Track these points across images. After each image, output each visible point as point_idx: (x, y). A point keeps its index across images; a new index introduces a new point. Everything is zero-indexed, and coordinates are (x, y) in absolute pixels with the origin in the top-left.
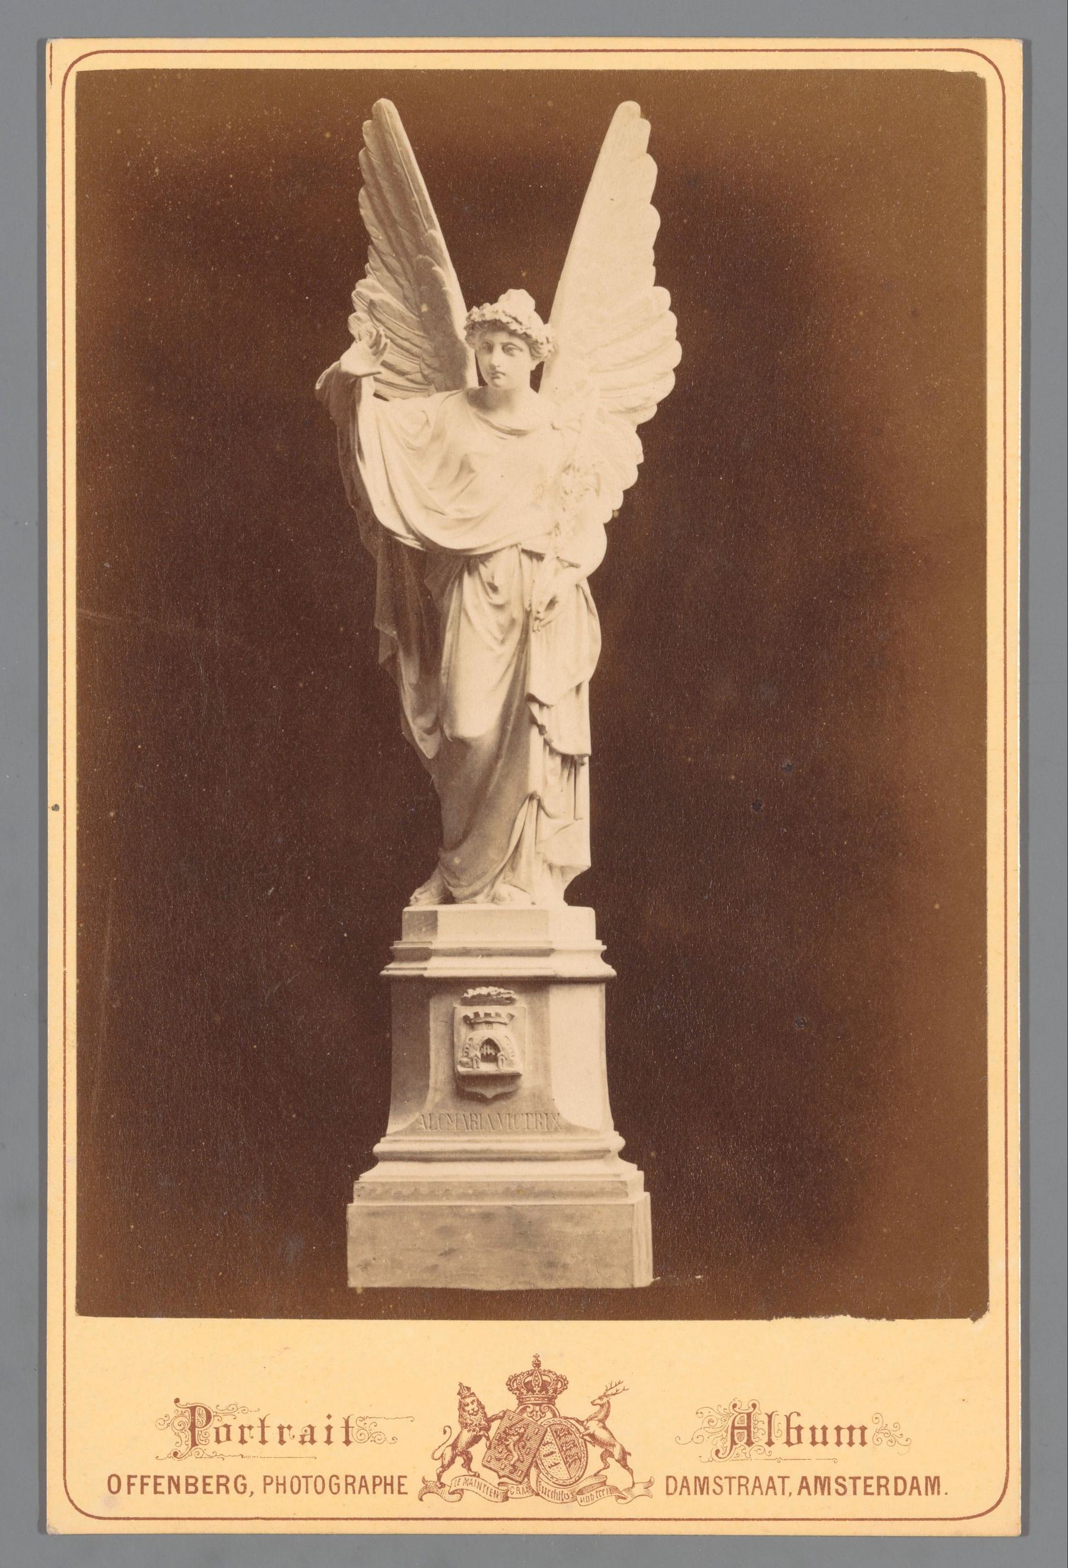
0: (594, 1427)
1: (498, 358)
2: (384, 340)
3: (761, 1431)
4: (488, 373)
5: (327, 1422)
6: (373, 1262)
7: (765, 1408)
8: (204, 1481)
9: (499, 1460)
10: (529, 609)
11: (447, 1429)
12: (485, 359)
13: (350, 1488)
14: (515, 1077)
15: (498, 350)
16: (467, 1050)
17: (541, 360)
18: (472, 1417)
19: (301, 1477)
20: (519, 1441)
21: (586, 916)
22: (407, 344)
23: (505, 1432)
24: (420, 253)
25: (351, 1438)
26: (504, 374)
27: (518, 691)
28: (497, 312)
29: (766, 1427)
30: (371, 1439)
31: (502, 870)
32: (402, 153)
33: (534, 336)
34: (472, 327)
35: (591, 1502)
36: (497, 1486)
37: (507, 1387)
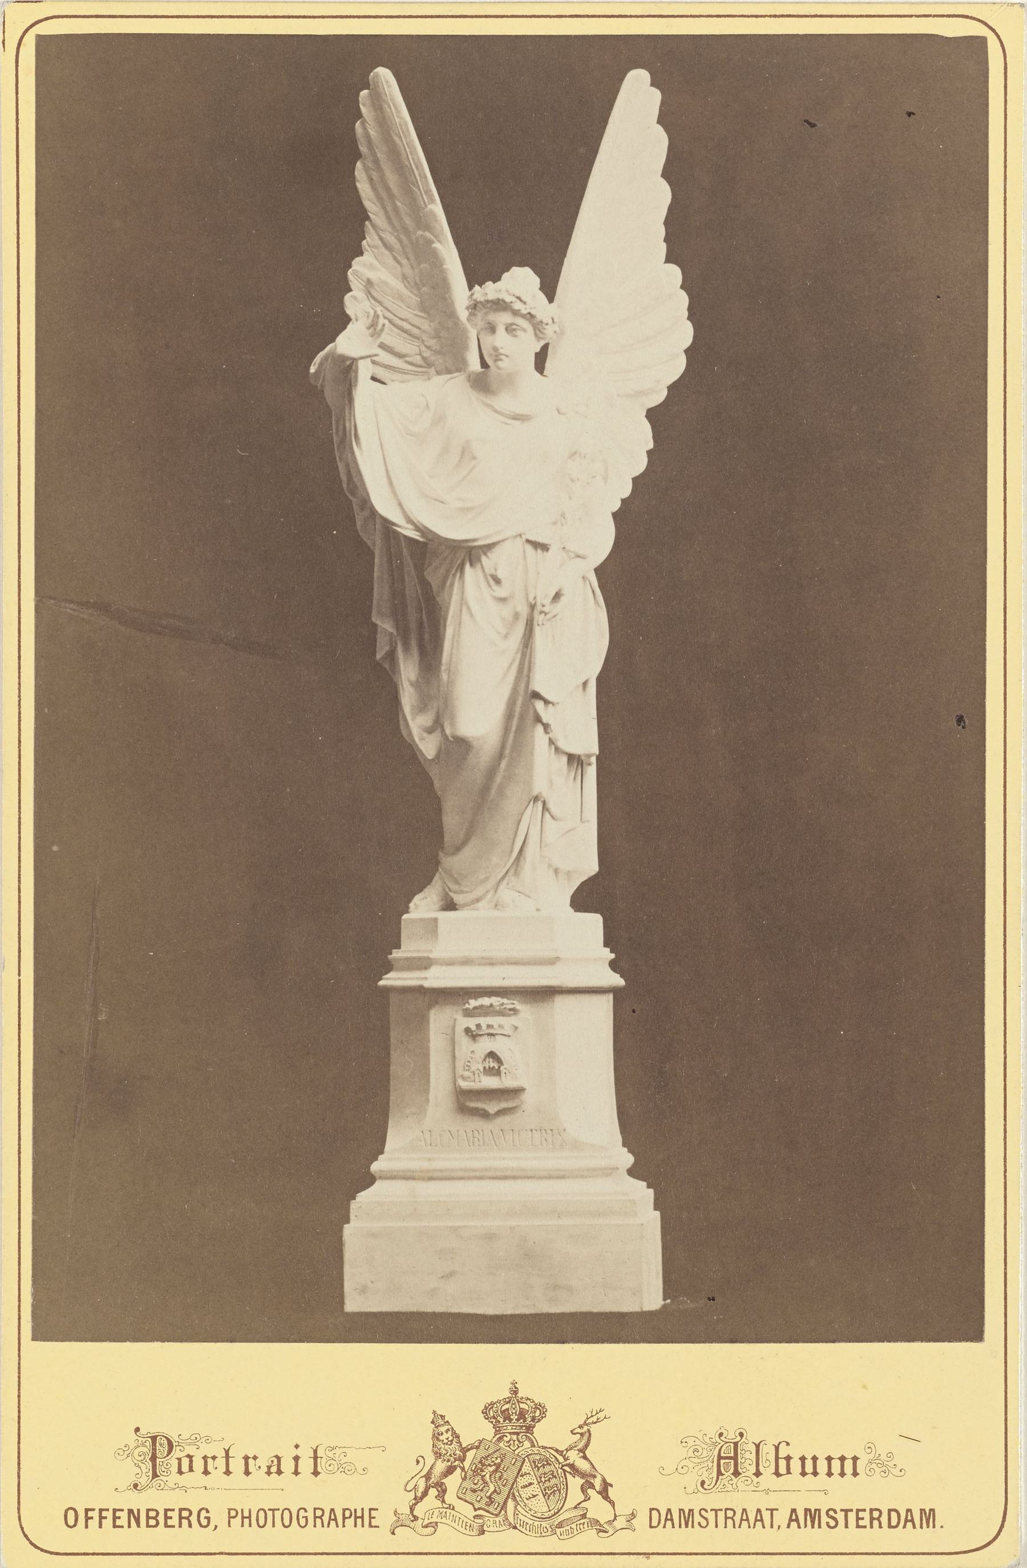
0: (574, 1456)
1: (501, 339)
2: (382, 321)
3: (749, 1462)
4: (491, 355)
5: (295, 1452)
6: (371, 1284)
7: (752, 1437)
8: (166, 1514)
9: (474, 1491)
10: (533, 603)
11: (420, 1459)
12: (488, 341)
13: (318, 1521)
14: (516, 1092)
15: (501, 330)
16: (468, 1064)
17: (546, 342)
18: (447, 1447)
19: (267, 1510)
20: (496, 1471)
22: (406, 326)
23: (480, 1462)
24: (419, 229)
25: (319, 1469)
26: (507, 356)
27: (523, 686)
28: (500, 290)
29: (753, 1456)
30: (341, 1469)
31: (507, 873)
32: (400, 125)
33: (539, 316)
34: (474, 307)
35: (571, 1536)
36: (473, 1519)
37: (483, 1415)
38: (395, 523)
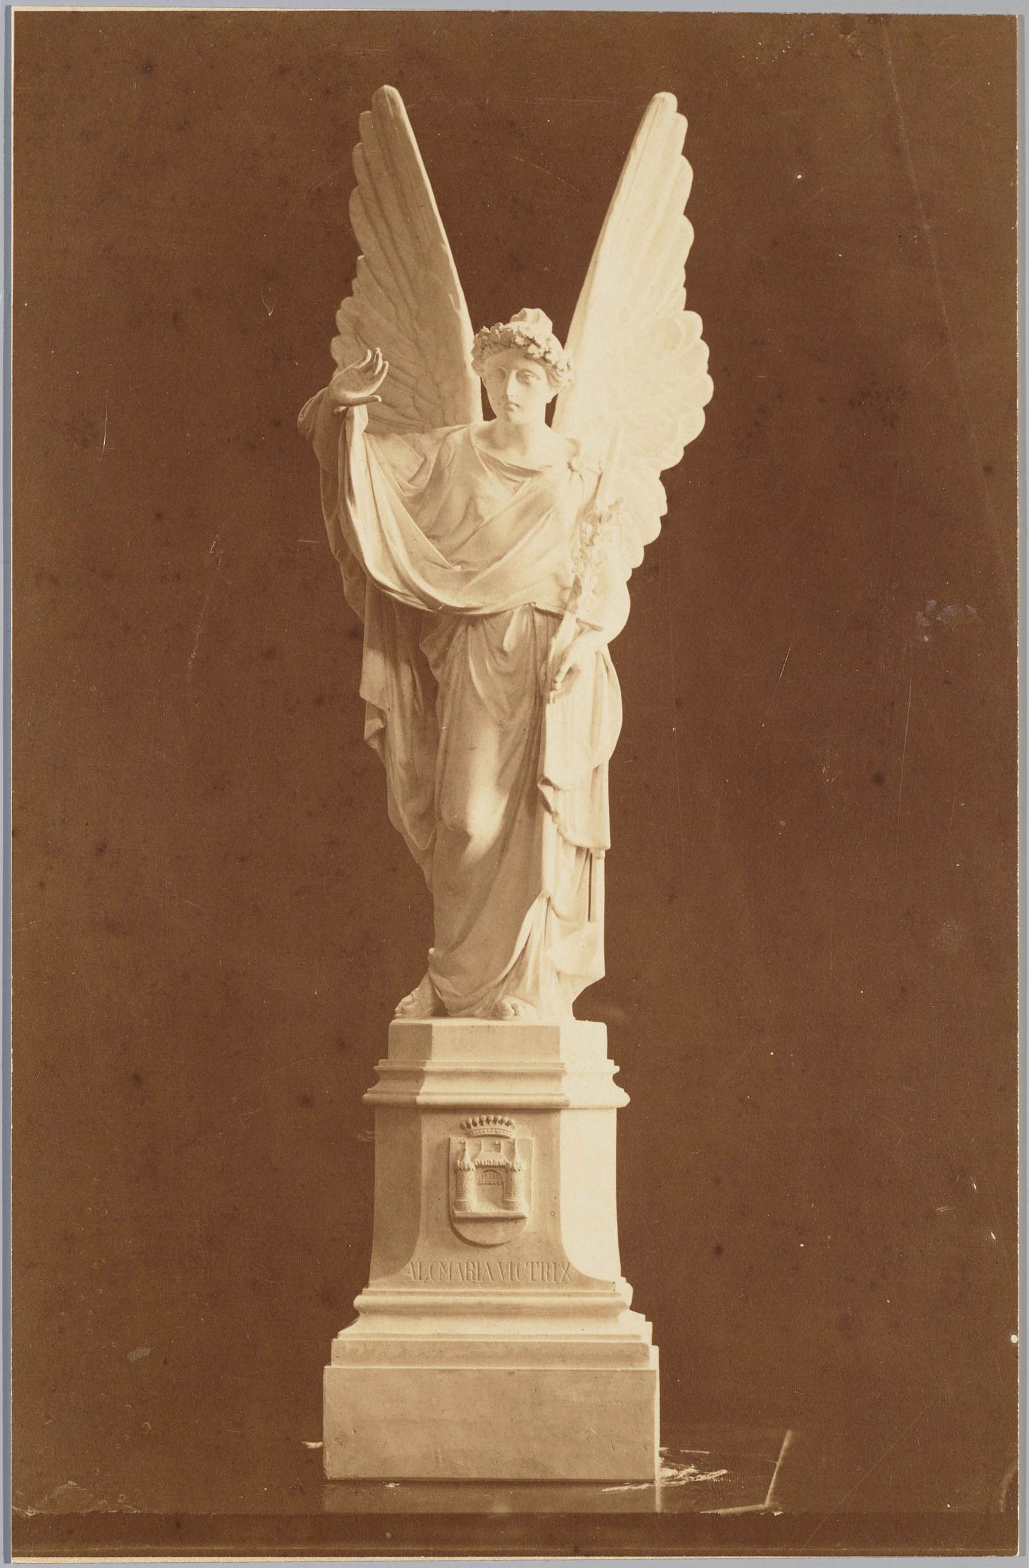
21: (597, 1032)
38: (389, 588)
